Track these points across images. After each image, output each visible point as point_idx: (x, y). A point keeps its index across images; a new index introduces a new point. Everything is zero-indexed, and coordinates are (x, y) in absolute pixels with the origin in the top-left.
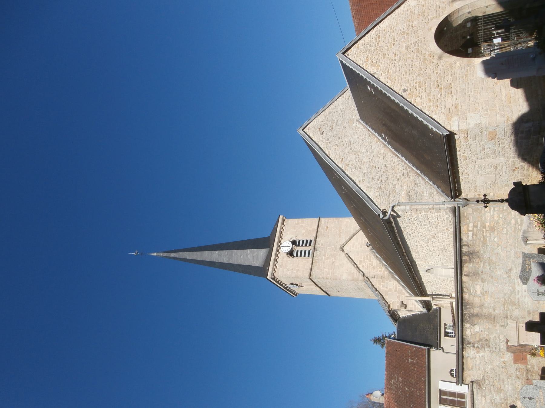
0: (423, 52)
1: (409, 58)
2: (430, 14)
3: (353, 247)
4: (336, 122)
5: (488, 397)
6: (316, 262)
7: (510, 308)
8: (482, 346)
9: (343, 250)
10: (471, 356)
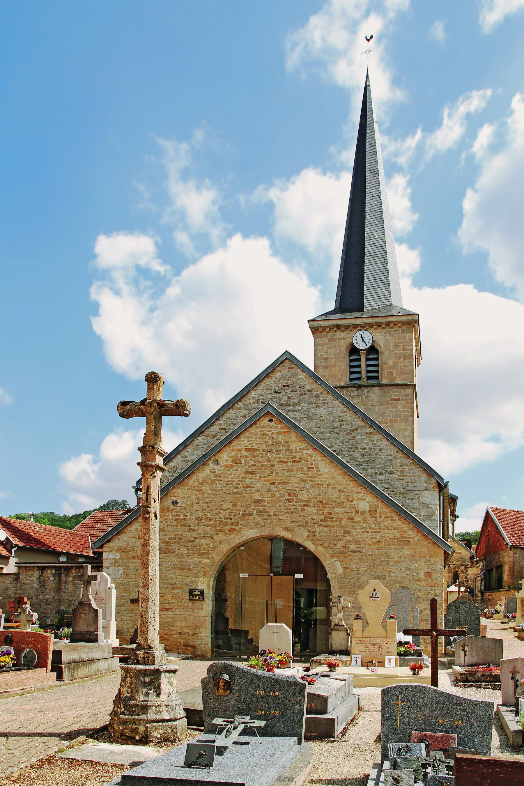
2: (326, 529)
4: (296, 408)
5: (10, 585)
7: (66, 604)
8: (40, 582)
10: (35, 573)
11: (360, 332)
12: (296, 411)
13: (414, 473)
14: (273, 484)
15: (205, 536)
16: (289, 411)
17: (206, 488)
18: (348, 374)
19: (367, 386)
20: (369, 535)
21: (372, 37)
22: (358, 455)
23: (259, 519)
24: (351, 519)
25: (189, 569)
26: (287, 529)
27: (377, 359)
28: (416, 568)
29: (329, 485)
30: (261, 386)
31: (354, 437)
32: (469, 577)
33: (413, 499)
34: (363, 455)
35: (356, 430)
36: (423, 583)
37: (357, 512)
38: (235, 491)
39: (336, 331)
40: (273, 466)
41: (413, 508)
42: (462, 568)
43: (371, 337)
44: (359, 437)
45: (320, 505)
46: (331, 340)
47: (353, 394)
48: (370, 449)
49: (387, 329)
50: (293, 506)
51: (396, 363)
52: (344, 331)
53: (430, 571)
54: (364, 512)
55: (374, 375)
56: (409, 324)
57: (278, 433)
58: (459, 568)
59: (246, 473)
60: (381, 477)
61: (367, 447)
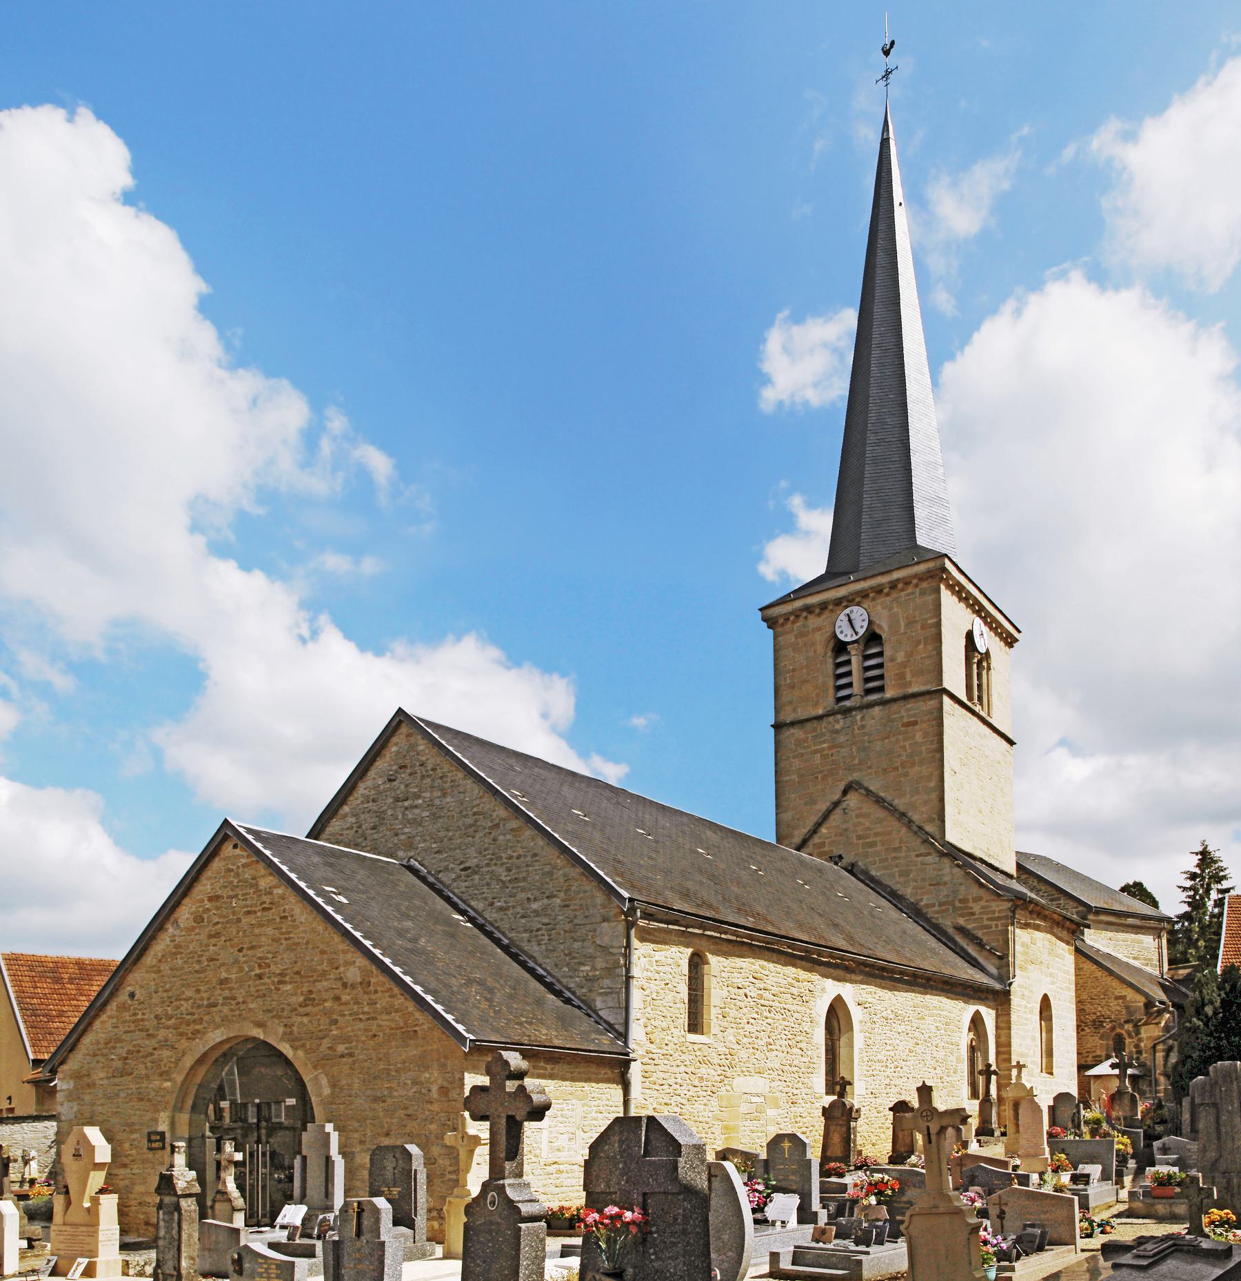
0: (206, 1018)
1: (198, 991)
2: (305, 1020)
3: (857, 816)
6: (815, 730)
9: (845, 792)
11: (847, 611)
12: (416, 807)
13: (585, 892)
14: (240, 950)
15: (165, 1044)
16: (406, 808)
17: (165, 967)
18: (831, 691)
19: (861, 708)
20: (361, 1025)
21: (893, 43)
22: (501, 871)
23: (226, 1009)
24: (337, 999)
25: (149, 1100)
26: (260, 1025)
27: (880, 654)
28: (428, 1081)
29: (307, 943)
30: (372, 774)
31: (495, 840)
32: (1142, 1044)
33: (584, 941)
34: (509, 870)
35: (497, 826)
36: (435, 1107)
37: (345, 985)
38: (198, 967)
39: (806, 618)
40: (239, 920)
41: (585, 956)
42: (1129, 1027)
43: (866, 616)
44: (501, 837)
45: (297, 978)
46: (802, 634)
47: (838, 727)
48: (519, 857)
49: (894, 595)
50: (264, 984)
51: (909, 655)
52: (819, 615)
53: (446, 1084)
54: (353, 986)
55: (874, 684)
56: (931, 577)
57: (244, 866)
58: (1121, 1026)
59: (210, 936)
60: (535, 906)
61: (515, 854)
